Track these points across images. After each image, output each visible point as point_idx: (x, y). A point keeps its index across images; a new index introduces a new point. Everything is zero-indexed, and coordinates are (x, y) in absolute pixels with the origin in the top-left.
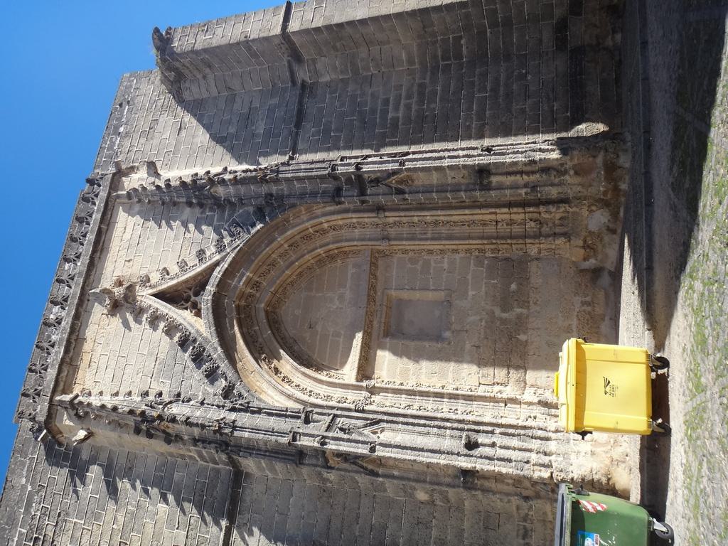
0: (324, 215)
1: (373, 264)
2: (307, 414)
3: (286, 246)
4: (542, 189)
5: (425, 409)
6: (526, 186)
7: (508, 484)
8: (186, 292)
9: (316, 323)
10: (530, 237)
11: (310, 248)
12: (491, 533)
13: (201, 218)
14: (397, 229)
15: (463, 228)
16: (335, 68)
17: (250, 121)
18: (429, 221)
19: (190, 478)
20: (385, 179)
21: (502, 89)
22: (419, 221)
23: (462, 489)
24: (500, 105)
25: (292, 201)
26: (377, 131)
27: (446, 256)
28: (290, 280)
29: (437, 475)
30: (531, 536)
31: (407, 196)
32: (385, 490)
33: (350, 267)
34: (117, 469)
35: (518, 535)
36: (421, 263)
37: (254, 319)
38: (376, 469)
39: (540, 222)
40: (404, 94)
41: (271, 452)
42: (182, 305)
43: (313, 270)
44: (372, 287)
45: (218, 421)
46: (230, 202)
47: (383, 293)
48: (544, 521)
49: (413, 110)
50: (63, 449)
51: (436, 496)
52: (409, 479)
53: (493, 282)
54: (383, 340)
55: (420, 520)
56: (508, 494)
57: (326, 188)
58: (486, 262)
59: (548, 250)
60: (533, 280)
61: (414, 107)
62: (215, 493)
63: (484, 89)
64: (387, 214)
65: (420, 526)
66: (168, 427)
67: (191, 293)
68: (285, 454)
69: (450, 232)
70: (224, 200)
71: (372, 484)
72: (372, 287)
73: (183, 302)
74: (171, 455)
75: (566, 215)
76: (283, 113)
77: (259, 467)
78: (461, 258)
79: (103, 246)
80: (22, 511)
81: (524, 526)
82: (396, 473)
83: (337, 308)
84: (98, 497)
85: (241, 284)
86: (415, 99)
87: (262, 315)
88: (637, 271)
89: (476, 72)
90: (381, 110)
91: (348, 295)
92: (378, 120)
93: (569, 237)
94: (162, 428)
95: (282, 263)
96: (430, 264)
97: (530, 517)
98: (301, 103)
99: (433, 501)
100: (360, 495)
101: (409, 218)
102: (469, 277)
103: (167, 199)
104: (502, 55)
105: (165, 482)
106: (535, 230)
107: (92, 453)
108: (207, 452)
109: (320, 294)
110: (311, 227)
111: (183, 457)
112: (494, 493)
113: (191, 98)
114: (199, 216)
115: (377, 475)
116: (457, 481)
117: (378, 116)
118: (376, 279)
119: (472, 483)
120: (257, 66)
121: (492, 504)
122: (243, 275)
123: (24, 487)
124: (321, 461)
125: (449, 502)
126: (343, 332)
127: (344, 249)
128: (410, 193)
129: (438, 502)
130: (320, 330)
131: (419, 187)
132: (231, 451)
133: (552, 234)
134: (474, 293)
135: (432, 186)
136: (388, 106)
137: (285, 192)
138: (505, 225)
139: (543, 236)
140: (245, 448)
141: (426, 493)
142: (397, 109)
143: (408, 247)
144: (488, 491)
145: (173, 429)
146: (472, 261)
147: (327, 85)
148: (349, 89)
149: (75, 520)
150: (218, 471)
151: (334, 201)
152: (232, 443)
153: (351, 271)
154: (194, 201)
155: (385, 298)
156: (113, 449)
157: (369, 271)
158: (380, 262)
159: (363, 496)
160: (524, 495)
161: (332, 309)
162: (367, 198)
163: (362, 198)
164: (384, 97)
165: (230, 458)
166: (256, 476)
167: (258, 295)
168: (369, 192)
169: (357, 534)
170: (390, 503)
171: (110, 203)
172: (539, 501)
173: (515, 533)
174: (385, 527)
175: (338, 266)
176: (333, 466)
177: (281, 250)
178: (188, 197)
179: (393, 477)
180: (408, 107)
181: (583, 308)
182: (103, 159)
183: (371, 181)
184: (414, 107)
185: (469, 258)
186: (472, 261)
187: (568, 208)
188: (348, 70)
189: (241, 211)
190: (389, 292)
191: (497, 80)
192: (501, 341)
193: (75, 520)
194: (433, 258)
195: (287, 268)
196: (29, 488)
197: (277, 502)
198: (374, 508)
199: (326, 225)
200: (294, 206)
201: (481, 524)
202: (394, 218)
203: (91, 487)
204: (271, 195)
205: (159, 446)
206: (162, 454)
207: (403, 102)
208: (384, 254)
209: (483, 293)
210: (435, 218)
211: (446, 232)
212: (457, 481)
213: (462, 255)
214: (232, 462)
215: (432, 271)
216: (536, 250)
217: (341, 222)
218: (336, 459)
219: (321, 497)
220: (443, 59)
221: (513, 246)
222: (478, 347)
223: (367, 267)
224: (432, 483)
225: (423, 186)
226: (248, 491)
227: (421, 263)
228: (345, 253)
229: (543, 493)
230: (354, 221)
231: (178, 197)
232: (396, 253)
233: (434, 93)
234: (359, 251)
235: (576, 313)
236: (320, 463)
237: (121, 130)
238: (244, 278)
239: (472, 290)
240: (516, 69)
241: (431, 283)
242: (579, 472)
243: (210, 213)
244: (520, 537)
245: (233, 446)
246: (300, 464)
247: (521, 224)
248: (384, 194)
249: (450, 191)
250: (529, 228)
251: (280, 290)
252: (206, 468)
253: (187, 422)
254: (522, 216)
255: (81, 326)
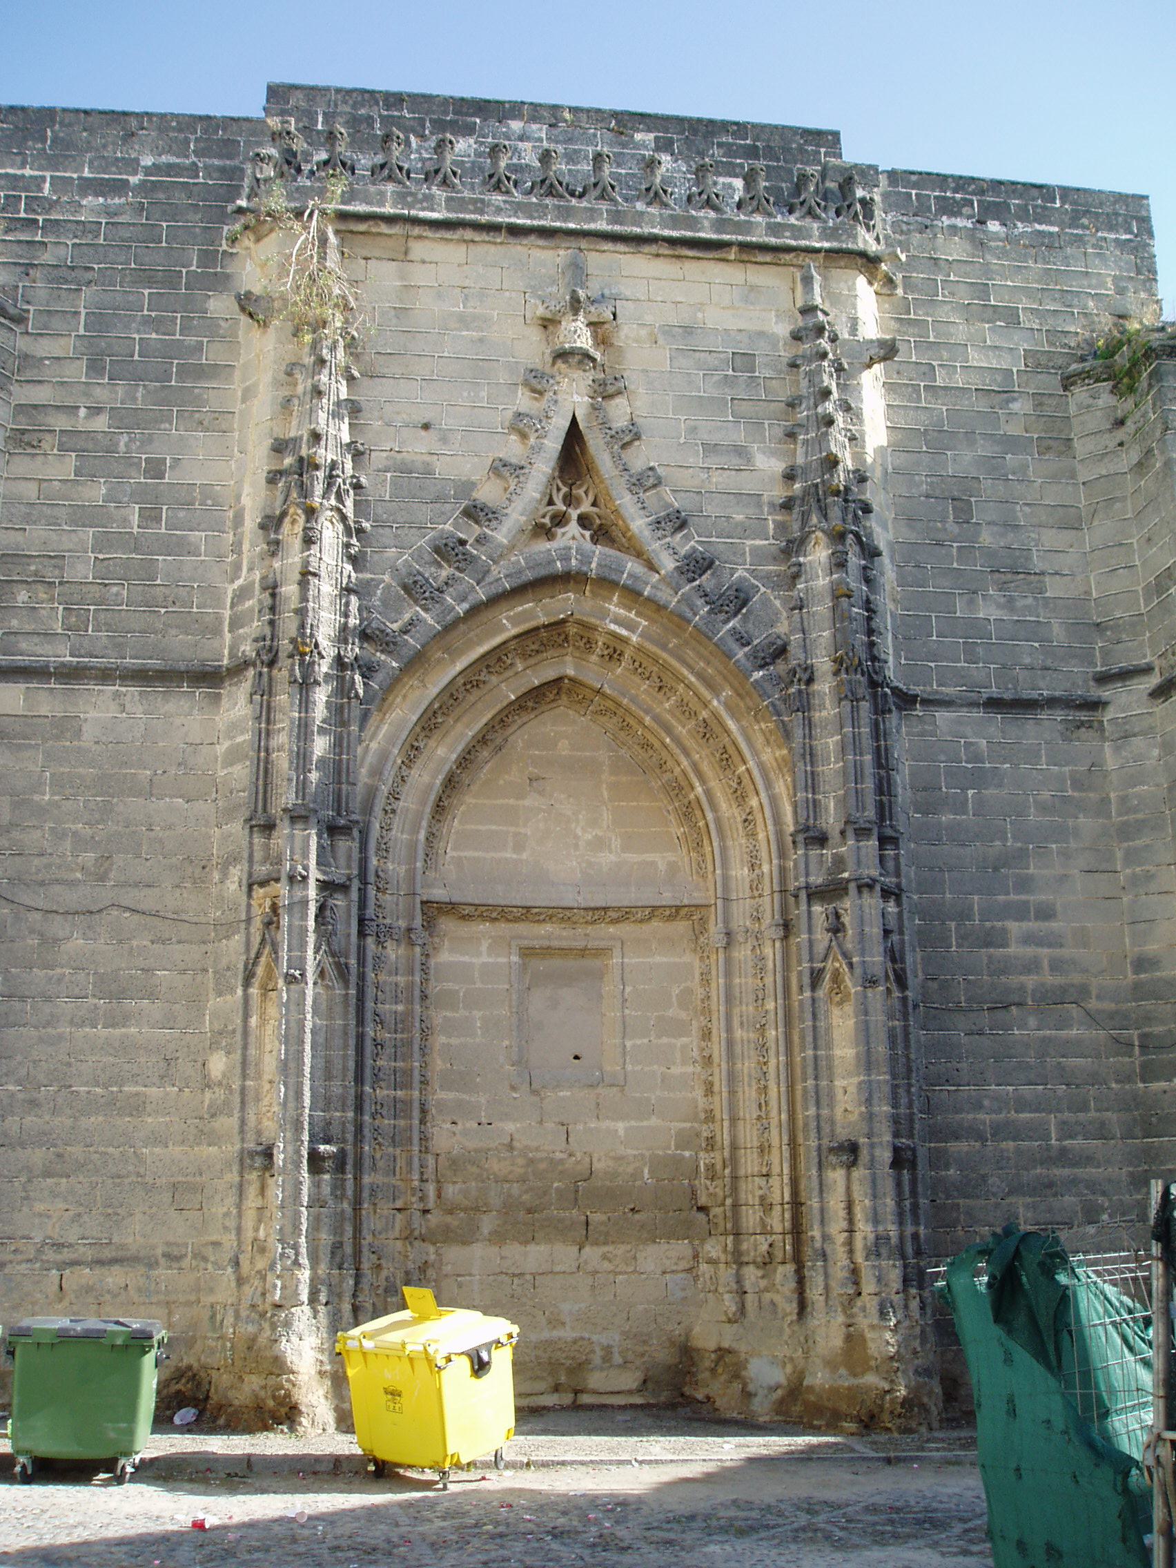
0: (774, 800)
1: (675, 912)
2: (345, 830)
3: (704, 714)
4: (821, 1271)
5: (377, 1054)
6: (826, 1237)
7: (257, 1230)
8: (586, 493)
9: (541, 793)
10: (737, 1243)
11: (705, 767)
12: (166, 1197)
13: (759, 505)
14: (751, 964)
15: (755, 1106)
16: (1134, 781)
17: (1009, 577)
18: (767, 1034)
19: (195, 569)
20: (840, 946)
21: (1066, 1172)
22: (767, 1012)
23: (238, 1147)
24: (1026, 1169)
25: (798, 733)
26: (976, 897)
27: (699, 1069)
28: (632, 722)
29: (258, 1099)
30: (170, 1268)
31: (807, 994)
32: (220, 994)
33: (671, 857)
34: (196, 391)
35: (168, 1244)
36: (683, 1015)
37: (540, 657)
38: (256, 982)
39: (767, 1263)
40: (1066, 952)
41: (267, 761)
42: (559, 489)
43: (658, 771)
44: (624, 914)
45: (317, 646)
46: (795, 577)
47: (612, 938)
48: (199, 1290)
49: (1023, 978)
50: (225, 247)
51: (220, 1093)
52: (245, 1047)
53: (646, 1171)
54: (514, 950)
55: (173, 1063)
56: (239, 1230)
57: (827, 809)
58: (687, 1154)
59: (714, 1279)
60: (651, 1249)
61: (1030, 981)
62: (173, 632)
63: (1067, 1131)
64: (778, 944)
65: (163, 1064)
66: (294, 522)
67: (586, 507)
68: (265, 792)
69: (746, 1079)
70: (800, 565)
71: (228, 969)
72: (624, 914)
73: (565, 489)
74: (238, 520)
75: (780, 1316)
76: (1027, 660)
77: (234, 728)
78: (695, 1101)
79: (687, 257)
80: (86, 173)
81: (186, 1255)
82: (253, 1021)
83: (576, 837)
84: (136, 357)
85: (613, 627)
86: (1050, 979)
87: (550, 674)
88: (812, 1449)
89: (1109, 1113)
90: (1028, 902)
91: (607, 859)
92: (1001, 898)
93: (736, 1322)
94: (291, 511)
95: (667, 705)
96: (681, 1036)
97: (202, 1265)
98: (1052, 702)
99: (209, 1087)
100: (204, 943)
101: (772, 993)
102: (654, 1121)
103: (803, 414)
104: (1146, 1167)
105: (181, 514)
106: (752, 1254)
107: (222, 323)
108: (251, 610)
109: (605, 794)
110: (747, 770)
111: (237, 548)
112: (239, 1206)
113: (1073, 410)
114: (765, 499)
115: (247, 983)
116: (251, 1136)
117: (1012, 897)
118: (641, 921)
119: (252, 1167)
120: (1143, 585)
121: (218, 1198)
122: (631, 627)
123: (133, 165)
124: (262, 870)
125: (212, 1116)
126: (524, 856)
127: (706, 842)
128: (813, 1000)
129: (208, 1095)
130: (527, 802)
131: (826, 1017)
132: (260, 674)
133: (742, 1287)
134: (621, 1133)
135: (829, 1046)
136: (1037, 918)
137: (817, 714)
138: (761, 1192)
139: (738, 1271)
140: (269, 703)
141: (224, 1075)
142: (1028, 939)
143: (714, 985)
144: (241, 1195)
145: (291, 532)
146: (689, 1125)
147: (1096, 765)
148: (1082, 820)
149: (83, 312)
150: (217, 632)
151: (797, 832)
152: (275, 672)
153: (660, 860)
154: (797, 486)
155: (602, 944)
156: (237, 375)
157: (658, 904)
158: (681, 926)
159: (204, 948)
160: (241, 1257)
161: (573, 826)
162: (804, 907)
163: (803, 895)
164: (1059, 908)
165: (246, 664)
166: (217, 718)
167: (594, 658)
168: (817, 909)
169: (135, 943)
170: (196, 1002)
171: (792, 255)
172: (233, 1284)
173: (171, 1239)
174: (152, 996)
175: (671, 830)
176: (254, 894)
177: (694, 704)
178: (805, 469)
179: (246, 1017)
180: (1032, 966)
181: (597, 1349)
182: (914, 192)
183: (837, 916)
184: (1030, 981)
185: (695, 1118)
186: (689, 1125)
187: (789, 1319)
188: (1127, 813)
189: (777, 603)
190: (617, 952)
191: (1089, 1160)
192: (526, 1192)
193: (83, 312)
194: (691, 1041)
195: (656, 719)
196: (134, 180)
197: (173, 771)
198: (183, 972)
199: (754, 802)
200: (787, 734)
201: (180, 1179)
202: (771, 956)
203: (154, 336)
204: (810, 681)
205: (253, 499)
206: (238, 498)
207: (1044, 952)
208: (701, 928)
209: (622, 1151)
210: (773, 1046)
211: (746, 1071)
212: (251, 1136)
213: (702, 1102)
214: (239, 668)
215: (665, 1040)
216: (714, 1254)
217: (761, 836)
218: (268, 903)
219: (192, 862)
220: (1144, 1036)
221: (722, 1209)
222: (510, 1147)
223: (667, 898)
224: (243, 1090)
225: (829, 1029)
226: (185, 704)
227: (683, 1015)
228: (700, 844)
229: (247, 1290)
230: (766, 868)
231: (806, 442)
232: (702, 959)
233: (1063, 1024)
234: (704, 877)
235: (587, 1336)
236: (256, 867)
237: (994, 226)
238: (624, 632)
239: (626, 1129)
240: (1110, 1200)
241: (639, 1042)
242: (289, 1351)
243: (771, 526)
244: (166, 1250)
245: (270, 679)
246: (252, 827)
247: (763, 1224)
248: (811, 942)
249: (817, 1085)
250: (755, 1240)
251: (609, 704)
252: (218, 602)
253: (306, 575)
254: (778, 1228)
255: (495, 243)
